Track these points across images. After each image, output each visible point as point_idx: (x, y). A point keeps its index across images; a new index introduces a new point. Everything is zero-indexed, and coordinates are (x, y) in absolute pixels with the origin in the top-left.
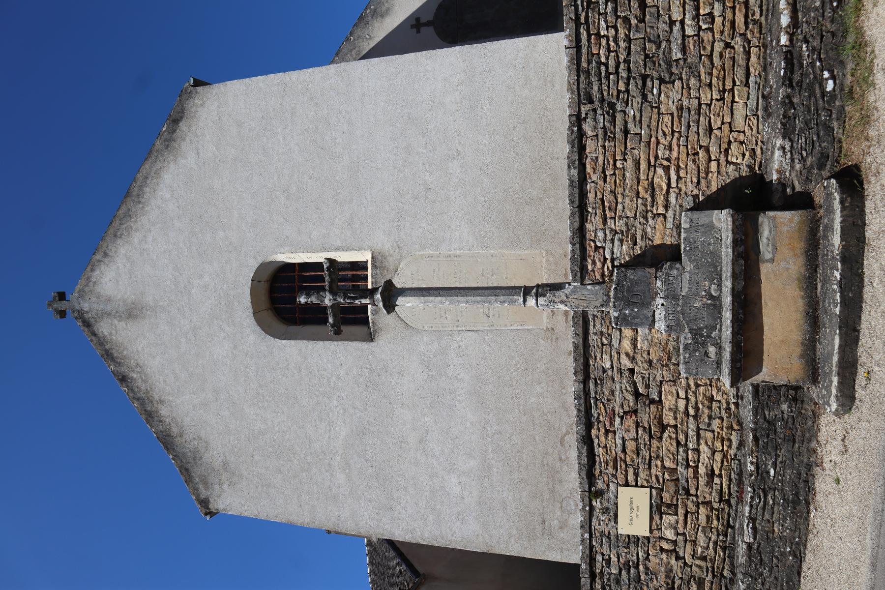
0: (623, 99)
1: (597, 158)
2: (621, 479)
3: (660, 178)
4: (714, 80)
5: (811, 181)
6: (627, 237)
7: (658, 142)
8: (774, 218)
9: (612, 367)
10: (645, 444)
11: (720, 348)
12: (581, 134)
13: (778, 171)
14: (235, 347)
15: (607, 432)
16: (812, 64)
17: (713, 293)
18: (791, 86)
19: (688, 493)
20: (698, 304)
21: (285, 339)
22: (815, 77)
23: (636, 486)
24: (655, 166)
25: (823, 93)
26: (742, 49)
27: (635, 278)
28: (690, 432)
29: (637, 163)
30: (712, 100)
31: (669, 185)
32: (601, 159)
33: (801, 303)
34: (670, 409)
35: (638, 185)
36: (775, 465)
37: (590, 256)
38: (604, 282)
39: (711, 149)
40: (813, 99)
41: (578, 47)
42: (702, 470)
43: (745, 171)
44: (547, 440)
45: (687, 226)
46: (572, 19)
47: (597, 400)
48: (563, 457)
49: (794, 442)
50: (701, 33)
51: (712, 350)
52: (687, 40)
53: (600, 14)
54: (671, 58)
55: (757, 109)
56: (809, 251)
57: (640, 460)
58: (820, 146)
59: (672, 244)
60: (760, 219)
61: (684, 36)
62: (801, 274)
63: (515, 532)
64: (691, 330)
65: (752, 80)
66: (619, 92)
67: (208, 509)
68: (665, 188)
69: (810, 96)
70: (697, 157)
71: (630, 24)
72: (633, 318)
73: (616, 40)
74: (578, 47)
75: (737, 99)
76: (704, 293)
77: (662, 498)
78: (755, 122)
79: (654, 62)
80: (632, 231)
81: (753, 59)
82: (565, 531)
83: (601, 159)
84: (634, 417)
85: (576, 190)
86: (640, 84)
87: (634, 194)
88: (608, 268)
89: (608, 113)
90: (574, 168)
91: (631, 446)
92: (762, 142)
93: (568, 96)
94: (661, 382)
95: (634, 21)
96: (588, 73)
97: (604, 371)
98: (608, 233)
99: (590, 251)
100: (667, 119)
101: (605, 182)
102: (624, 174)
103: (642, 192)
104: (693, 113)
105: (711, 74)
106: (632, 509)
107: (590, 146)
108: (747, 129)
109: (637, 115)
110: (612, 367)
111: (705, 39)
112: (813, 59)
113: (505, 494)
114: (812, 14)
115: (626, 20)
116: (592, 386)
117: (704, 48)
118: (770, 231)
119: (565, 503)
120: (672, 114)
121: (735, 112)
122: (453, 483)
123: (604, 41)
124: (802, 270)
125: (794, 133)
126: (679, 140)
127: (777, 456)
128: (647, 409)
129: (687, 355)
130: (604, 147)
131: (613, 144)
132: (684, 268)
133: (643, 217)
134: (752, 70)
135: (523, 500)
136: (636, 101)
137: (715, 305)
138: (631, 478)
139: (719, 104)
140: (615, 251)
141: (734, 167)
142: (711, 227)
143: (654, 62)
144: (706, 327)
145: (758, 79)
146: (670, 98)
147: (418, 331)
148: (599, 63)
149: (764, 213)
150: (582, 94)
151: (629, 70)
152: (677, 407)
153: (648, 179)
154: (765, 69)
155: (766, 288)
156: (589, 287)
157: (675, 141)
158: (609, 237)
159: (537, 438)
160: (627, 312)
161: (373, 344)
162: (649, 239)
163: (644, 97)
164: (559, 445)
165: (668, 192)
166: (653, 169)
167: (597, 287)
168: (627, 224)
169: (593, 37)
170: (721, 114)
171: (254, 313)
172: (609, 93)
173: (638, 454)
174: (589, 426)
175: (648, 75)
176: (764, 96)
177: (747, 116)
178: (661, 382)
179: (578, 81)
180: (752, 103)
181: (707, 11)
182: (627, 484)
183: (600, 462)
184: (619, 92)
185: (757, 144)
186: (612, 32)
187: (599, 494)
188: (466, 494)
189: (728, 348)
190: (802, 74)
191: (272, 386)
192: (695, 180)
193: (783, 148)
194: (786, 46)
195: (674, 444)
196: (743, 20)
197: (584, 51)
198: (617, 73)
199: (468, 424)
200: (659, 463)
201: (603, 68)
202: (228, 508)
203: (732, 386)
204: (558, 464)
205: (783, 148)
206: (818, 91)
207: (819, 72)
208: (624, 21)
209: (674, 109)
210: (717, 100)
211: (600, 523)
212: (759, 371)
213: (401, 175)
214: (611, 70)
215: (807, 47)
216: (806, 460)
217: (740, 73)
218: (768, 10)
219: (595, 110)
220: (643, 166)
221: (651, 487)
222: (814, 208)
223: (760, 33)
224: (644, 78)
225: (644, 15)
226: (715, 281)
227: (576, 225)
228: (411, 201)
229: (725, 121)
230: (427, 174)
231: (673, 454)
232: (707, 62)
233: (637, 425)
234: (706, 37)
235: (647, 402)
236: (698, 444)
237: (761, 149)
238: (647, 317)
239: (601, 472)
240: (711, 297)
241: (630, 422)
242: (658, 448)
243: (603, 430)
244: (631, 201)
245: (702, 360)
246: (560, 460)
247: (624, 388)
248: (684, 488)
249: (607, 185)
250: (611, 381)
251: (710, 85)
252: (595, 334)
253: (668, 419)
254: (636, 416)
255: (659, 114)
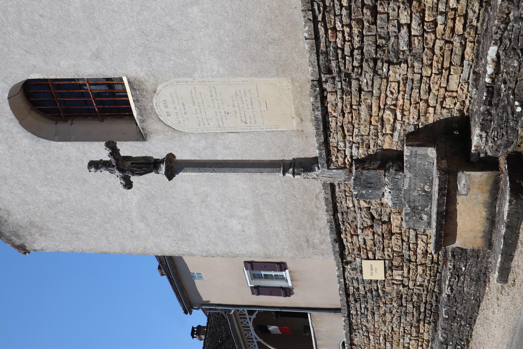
0: (358, 72)
1: (337, 104)
2: (364, 256)
3: (388, 115)
4: (435, 64)
5: (499, 152)
6: (363, 145)
7: (387, 96)
8: (469, 175)
9: (354, 206)
10: (379, 242)
11: (430, 217)
12: (323, 90)
13: (475, 146)
14: (10, 147)
15: (352, 236)
16: (508, 96)
17: (426, 190)
18: (490, 104)
19: (410, 261)
20: (416, 194)
21: (59, 140)
22: (509, 103)
23: (375, 259)
24: (384, 109)
25: (513, 113)
26: (459, 45)
27: (369, 175)
28: (411, 236)
29: (370, 107)
30: (432, 73)
31: (395, 119)
32: (340, 105)
33: (484, 214)
34: (397, 226)
35: (371, 118)
36: (465, 266)
37: (334, 154)
38: (345, 168)
39: (429, 101)
40: (505, 114)
41: (317, 38)
42: (419, 251)
43: (456, 114)
44: (305, 197)
45: (408, 154)
46: (310, 20)
47: (344, 221)
48: (319, 206)
49: (478, 258)
50: (425, 35)
51: (425, 217)
52: (413, 38)
53: (335, 15)
54: (398, 48)
55: (468, 79)
56: (492, 190)
57: (376, 249)
58: (507, 137)
59: (397, 150)
60: (460, 174)
61: (410, 36)
62: (486, 201)
63: (287, 247)
64: (409, 206)
65: (465, 62)
66: (354, 67)
67: (25, 250)
68: (392, 120)
69: (503, 112)
70: (418, 105)
71: (363, 25)
72: (369, 195)
73: (351, 34)
74: (317, 38)
75: (452, 73)
76: (419, 189)
77: (392, 264)
78: (466, 86)
79: (384, 51)
80: (367, 142)
81: (468, 50)
82: (325, 245)
83: (340, 105)
84: (371, 230)
85: (321, 124)
86: (372, 64)
87: (367, 124)
88: (348, 161)
89: (345, 81)
90: (318, 111)
91: (369, 243)
92: (471, 97)
93: (310, 69)
94: (390, 213)
95: (366, 24)
96: (327, 53)
97: (348, 208)
98: (347, 143)
99: (334, 151)
100: (395, 85)
101: (344, 117)
102: (359, 113)
103: (373, 122)
104: (415, 82)
105: (432, 60)
106: (372, 269)
107: (330, 98)
108: (459, 90)
109: (370, 83)
110: (354, 206)
111: (429, 38)
112: (508, 93)
113: (276, 228)
114: (511, 69)
115: (360, 22)
116: (339, 215)
117: (427, 44)
118: (466, 181)
119: (322, 230)
120: (399, 82)
121: (450, 81)
122: (234, 223)
123: (340, 35)
124: (487, 199)
125: (489, 129)
126: (403, 95)
127: (467, 262)
128: (381, 227)
129: (407, 218)
130: (342, 98)
131: (350, 97)
132: (405, 176)
133: (375, 136)
134: (466, 56)
135: (291, 230)
136: (369, 75)
137: (428, 196)
138: (370, 255)
139: (437, 77)
140: (353, 152)
141: (447, 111)
142: (426, 156)
143: (384, 51)
144: (421, 206)
145: (471, 63)
146: (397, 73)
147: (186, 134)
148: (336, 48)
149: (463, 171)
150: (322, 67)
151: (362, 54)
152: (401, 225)
153: (378, 116)
154: (477, 56)
155: (460, 207)
156: (334, 171)
157: (400, 97)
158: (348, 145)
159: (297, 196)
160: (364, 192)
161: (146, 143)
162: (380, 146)
163: (375, 72)
164: (315, 199)
165: (394, 122)
166: (382, 111)
167: (340, 171)
168: (362, 139)
169: (330, 31)
170: (439, 82)
171: (21, 123)
172: (345, 67)
173: (375, 246)
174: (339, 232)
175: (379, 58)
176: (474, 73)
177: (460, 82)
178: (390, 213)
179: (318, 60)
180: (465, 75)
181: (431, 19)
182: (368, 259)
183: (349, 249)
184: (354, 67)
185: (466, 98)
186: (347, 30)
187: (348, 263)
188: (245, 229)
189: (434, 216)
190: (499, 100)
191: (59, 173)
192: (416, 117)
193: (481, 136)
194: (488, 84)
195: (400, 241)
196: (462, 27)
197: (323, 40)
198: (352, 55)
199: (241, 190)
200: (390, 249)
201: (339, 52)
202: (45, 249)
203: (435, 253)
204: (315, 210)
205: (481, 136)
206: (509, 110)
207: (511, 101)
208: (357, 23)
209: (400, 79)
210: (435, 74)
211: (350, 274)
212: (454, 242)
213: (141, 18)
214: (346, 53)
215: (505, 87)
216: (485, 266)
217: (456, 59)
218: (484, 20)
219: (333, 78)
220: (375, 109)
221: (385, 260)
222: (498, 170)
223: (476, 33)
224: (375, 61)
225: (376, 19)
226: (428, 184)
227: (322, 140)
228: (157, 39)
229: (442, 85)
230: (168, 18)
231: (399, 246)
232: (429, 52)
233: (374, 233)
234: (430, 37)
235: (380, 223)
236: (417, 240)
237: (470, 101)
238: (379, 195)
239: (349, 253)
240: (425, 191)
241: (369, 232)
242: (389, 243)
243: (349, 235)
244: (365, 127)
245: (417, 221)
246: (317, 207)
247: (363, 216)
248: (407, 260)
249: (346, 119)
250: (354, 213)
251: (431, 65)
252: (340, 192)
253: (395, 230)
254: (372, 229)
255: (388, 82)
